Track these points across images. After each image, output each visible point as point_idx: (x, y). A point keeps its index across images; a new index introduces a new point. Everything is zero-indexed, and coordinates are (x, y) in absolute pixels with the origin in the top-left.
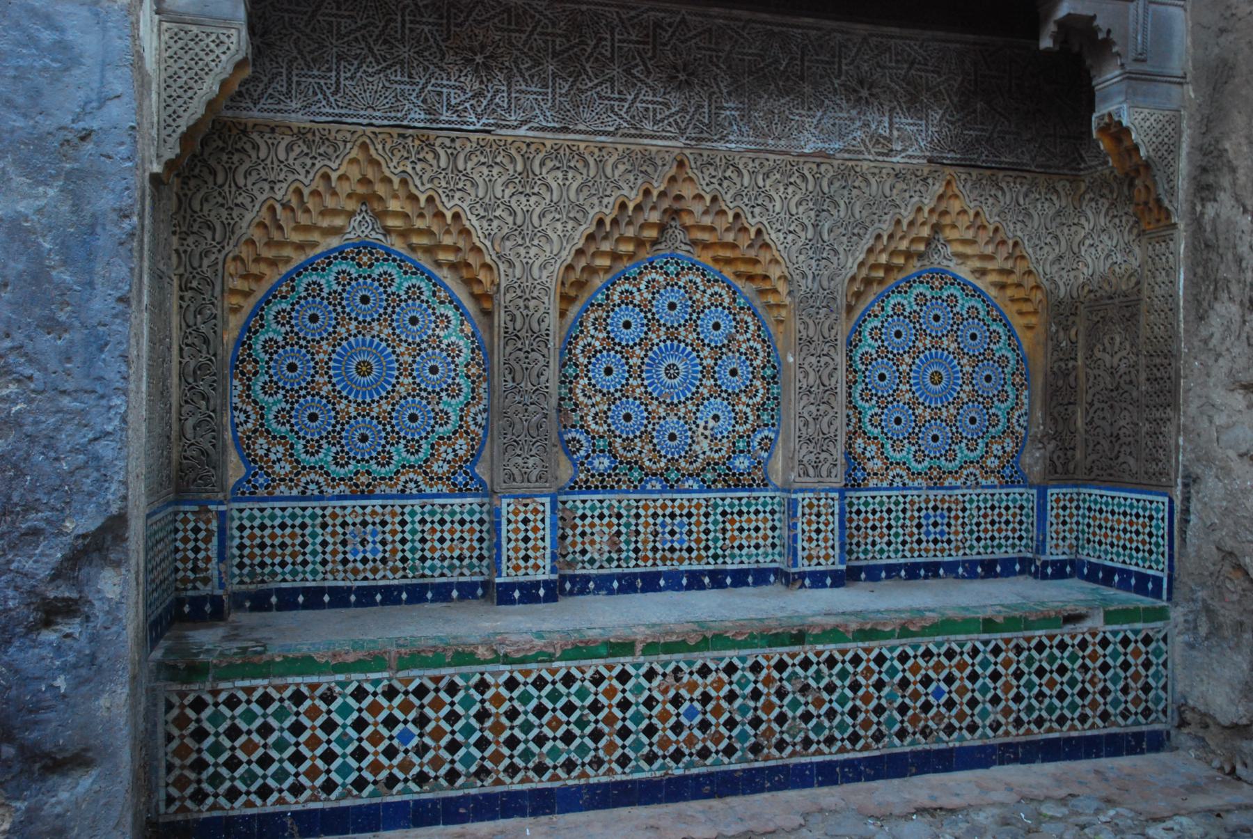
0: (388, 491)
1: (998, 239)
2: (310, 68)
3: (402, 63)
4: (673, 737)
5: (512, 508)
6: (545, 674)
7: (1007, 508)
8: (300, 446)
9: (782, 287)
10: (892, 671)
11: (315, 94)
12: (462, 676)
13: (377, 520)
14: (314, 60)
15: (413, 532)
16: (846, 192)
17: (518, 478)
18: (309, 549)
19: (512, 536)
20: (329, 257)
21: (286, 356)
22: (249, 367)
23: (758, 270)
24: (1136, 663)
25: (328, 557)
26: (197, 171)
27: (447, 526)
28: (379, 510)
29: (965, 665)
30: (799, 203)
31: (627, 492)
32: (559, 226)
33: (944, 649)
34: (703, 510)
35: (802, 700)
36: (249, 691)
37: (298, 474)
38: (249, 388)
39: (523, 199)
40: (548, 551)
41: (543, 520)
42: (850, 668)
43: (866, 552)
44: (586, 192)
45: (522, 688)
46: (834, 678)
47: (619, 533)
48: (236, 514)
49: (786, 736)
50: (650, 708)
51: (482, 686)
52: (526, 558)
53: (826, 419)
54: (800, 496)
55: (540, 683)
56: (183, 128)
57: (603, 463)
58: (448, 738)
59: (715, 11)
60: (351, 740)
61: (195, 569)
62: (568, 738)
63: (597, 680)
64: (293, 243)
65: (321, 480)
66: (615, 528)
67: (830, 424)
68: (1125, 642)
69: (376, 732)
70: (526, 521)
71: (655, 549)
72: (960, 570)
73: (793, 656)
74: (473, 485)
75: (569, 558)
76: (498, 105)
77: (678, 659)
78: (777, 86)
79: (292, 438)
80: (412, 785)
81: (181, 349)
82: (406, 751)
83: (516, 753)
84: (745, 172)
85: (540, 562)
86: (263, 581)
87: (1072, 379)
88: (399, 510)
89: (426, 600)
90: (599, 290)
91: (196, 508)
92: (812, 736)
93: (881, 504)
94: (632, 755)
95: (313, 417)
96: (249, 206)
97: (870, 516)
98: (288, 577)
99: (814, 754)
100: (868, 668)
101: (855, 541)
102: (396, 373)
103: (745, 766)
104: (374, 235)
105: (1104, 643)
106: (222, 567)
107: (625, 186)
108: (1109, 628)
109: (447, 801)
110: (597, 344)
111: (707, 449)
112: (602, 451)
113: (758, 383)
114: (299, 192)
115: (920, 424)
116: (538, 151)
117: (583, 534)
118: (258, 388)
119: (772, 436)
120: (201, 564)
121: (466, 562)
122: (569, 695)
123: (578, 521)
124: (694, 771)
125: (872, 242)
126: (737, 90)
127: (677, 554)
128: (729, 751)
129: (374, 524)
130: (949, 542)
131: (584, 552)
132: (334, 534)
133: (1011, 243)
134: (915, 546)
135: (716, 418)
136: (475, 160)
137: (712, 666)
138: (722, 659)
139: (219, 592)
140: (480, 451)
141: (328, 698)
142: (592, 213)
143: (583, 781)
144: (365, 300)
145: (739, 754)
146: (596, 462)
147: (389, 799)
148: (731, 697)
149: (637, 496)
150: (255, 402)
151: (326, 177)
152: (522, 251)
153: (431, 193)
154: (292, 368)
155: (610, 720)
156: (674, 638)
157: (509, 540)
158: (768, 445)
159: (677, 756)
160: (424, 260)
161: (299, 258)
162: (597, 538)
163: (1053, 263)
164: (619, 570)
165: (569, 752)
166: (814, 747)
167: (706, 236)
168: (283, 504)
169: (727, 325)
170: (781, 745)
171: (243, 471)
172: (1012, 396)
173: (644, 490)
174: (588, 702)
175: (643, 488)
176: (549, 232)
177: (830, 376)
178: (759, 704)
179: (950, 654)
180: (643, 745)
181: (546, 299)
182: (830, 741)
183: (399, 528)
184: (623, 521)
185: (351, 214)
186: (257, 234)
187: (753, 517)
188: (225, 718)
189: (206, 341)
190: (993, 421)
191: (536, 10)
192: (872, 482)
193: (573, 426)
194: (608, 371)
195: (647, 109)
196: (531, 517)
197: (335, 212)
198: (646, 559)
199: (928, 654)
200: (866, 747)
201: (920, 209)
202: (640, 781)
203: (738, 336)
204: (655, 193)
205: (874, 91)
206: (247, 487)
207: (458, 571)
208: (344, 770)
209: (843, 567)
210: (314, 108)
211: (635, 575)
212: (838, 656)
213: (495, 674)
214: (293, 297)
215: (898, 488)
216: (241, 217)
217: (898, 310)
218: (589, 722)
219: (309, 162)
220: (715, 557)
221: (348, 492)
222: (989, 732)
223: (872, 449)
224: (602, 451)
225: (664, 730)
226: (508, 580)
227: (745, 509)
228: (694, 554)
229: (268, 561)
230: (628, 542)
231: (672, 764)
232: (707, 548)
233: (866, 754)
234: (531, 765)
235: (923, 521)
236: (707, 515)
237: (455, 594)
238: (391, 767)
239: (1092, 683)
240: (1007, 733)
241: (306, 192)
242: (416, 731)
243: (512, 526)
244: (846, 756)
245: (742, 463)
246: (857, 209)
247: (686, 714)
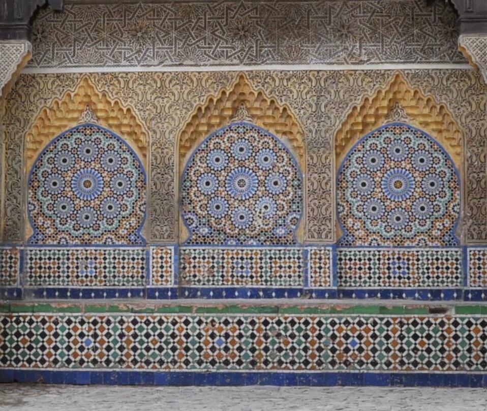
0: (98, 243)
2: (62, 46)
4: (211, 353)
6: (150, 318)
7: (447, 260)
9: (298, 137)
11: (64, 57)
12: (113, 317)
13: (93, 257)
14: (64, 42)
16: (334, 85)
18: (61, 270)
19: (155, 265)
21: (52, 179)
22: (36, 184)
23: (286, 129)
25: (70, 274)
27: (126, 261)
28: (94, 252)
29: (369, 330)
30: (308, 93)
32: (178, 112)
34: (259, 256)
35: (277, 341)
36: (25, 317)
37: (57, 234)
38: (35, 193)
39: (161, 100)
40: (173, 273)
41: (170, 258)
42: (303, 327)
43: (355, 282)
44: (192, 95)
45: (139, 324)
46: (295, 331)
47: (213, 267)
49: (269, 358)
50: (200, 338)
51: (122, 322)
52: (162, 276)
54: (309, 248)
55: (148, 323)
57: (205, 230)
58: (106, 344)
60: (65, 342)
61: (10, 276)
62: (161, 349)
64: (55, 126)
65: (67, 237)
66: (211, 265)
67: (327, 210)
69: (76, 339)
70: (162, 258)
71: (232, 276)
72: (417, 295)
73: (272, 318)
74: (139, 241)
75: (187, 279)
76: (148, 56)
77: (212, 316)
78: (294, 32)
79: (54, 217)
81: (6, 176)
82: (88, 349)
83: (137, 354)
85: (169, 279)
86: (40, 285)
88: (103, 252)
89: (115, 297)
90: (203, 143)
91: (10, 248)
92: (283, 359)
93: (364, 255)
94: (191, 360)
95: (64, 207)
96: (35, 110)
97: (358, 262)
98: (52, 283)
100: (313, 328)
101: (348, 275)
102: (102, 186)
103: (248, 371)
104: (92, 120)
106: (22, 275)
108: (458, 316)
110: (202, 170)
111: (261, 224)
112: (204, 224)
113: (290, 189)
114: (57, 103)
115: (388, 211)
116: (168, 76)
117: (194, 267)
120: (13, 274)
121: (135, 279)
122: (161, 329)
123: (192, 260)
124: (222, 371)
125: (350, 111)
126: (270, 37)
127: (244, 279)
128: (240, 363)
129: (91, 259)
130: (409, 278)
131: (195, 276)
132: (73, 263)
133: (438, 107)
134: (387, 280)
135: (266, 207)
136: (137, 83)
137: (230, 320)
139: (20, 287)
140: (143, 223)
141: (56, 323)
142: (195, 105)
143: (167, 370)
144: (88, 151)
145: (244, 364)
146: (201, 230)
147: (81, 370)
148: (240, 336)
149: (223, 248)
150: (38, 200)
151: (69, 95)
152: (160, 125)
153: (116, 100)
154: (55, 184)
155: (180, 342)
156: (211, 306)
157: (153, 267)
158: (295, 221)
159: (213, 363)
160: (116, 131)
161: (58, 133)
162: (202, 269)
163: (467, 117)
164: (214, 286)
165: (161, 356)
166: (284, 365)
167: (258, 113)
168: (50, 248)
169: (272, 158)
170: (266, 362)
172: (448, 194)
173: (226, 245)
174: (170, 333)
175: (226, 243)
176: (174, 116)
178: (255, 341)
179: (360, 324)
180: (196, 356)
181: (172, 148)
182: (293, 363)
183: (103, 261)
184: (215, 260)
185: (82, 111)
186: (38, 123)
188: (15, 328)
189: (16, 172)
190: (436, 209)
191: (166, 8)
192: (358, 243)
193: (190, 212)
194: (208, 184)
195: (223, 51)
197: (73, 111)
198: (228, 281)
199: (347, 323)
200: (313, 368)
201: (379, 92)
202: (194, 373)
203: (278, 164)
204: (228, 93)
205: (350, 30)
206: (34, 240)
207: (131, 283)
208: (62, 355)
209: (335, 288)
210: (64, 64)
211: (222, 289)
212: (296, 320)
213: (128, 317)
214: (55, 151)
215: (374, 247)
216: (32, 115)
217: (373, 148)
218: (170, 343)
219: (61, 89)
220: (266, 281)
221: (79, 243)
222: (385, 367)
224: (204, 224)
225: (206, 349)
226: (153, 287)
227: (282, 256)
228: (254, 279)
229: (43, 275)
230: (218, 272)
231: (211, 366)
232: (261, 276)
233: (313, 372)
234: (143, 360)
235: (391, 266)
236: (261, 259)
239: (448, 344)
240: (395, 368)
241: (60, 102)
243: (155, 260)
245: (280, 232)
246: (341, 94)
247: (217, 343)
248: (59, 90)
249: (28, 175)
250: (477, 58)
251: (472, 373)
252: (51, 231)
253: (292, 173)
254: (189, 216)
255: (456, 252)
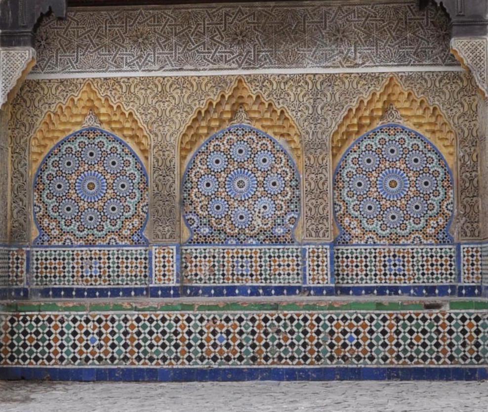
0: (102, 243)
1: (424, 106)
2: (65, 52)
3: (105, 46)
5: (157, 251)
6: (153, 316)
7: (441, 257)
8: (63, 222)
9: (296, 138)
10: (325, 326)
11: (68, 63)
12: (117, 315)
13: (97, 257)
15: (114, 263)
17: (160, 237)
18: (66, 270)
20: (75, 136)
22: (41, 187)
23: (285, 131)
24: (471, 331)
25: (75, 274)
26: (19, 102)
27: (129, 260)
28: (98, 252)
29: (366, 326)
30: (304, 96)
31: (218, 245)
32: (179, 115)
33: (354, 316)
34: (258, 255)
35: (277, 337)
36: (31, 316)
37: (61, 235)
38: (41, 196)
39: (162, 104)
40: (175, 272)
41: (172, 257)
42: (302, 323)
43: (352, 279)
45: (143, 322)
46: (294, 328)
47: (214, 266)
48: (35, 253)
49: (269, 354)
51: (126, 320)
52: (164, 275)
53: (321, 207)
54: (307, 247)
55: (151, 320)
56: (9, 91)
57: (206, 230)
59: (257, 4)
60: (71, 340)
61: (17, 276)
62: (164, 346)
63: (177, 321)
65: (72, 238)
66: (212, 263)
68: (463, 319)
69: (81, 337)
70: (164, 257)
71: (233, 275)
72: (412, 291)
74: (142, 241)
75: (189, 277)
76: (149, 61)
77: (214, 313)
78: (290, 37)
79: (59, 219)
80: (96, 362)
82: (93, 347)
84: (274, 82)
85: (171, 278)
87: (475, 182)
88: (107, 252)
90: (203, 145)
91: (17, 249)
92: (282, 355)
94: (193, 356)
97: (354, 260)
98: (57, 283)
99: (284, 364)
101: (345, 273)
102: (105, 188)
103: (248, 367)
104: (95, 124)
105: (450, 319)
106: (28, 275)
107: (211, 94)
109: (111, 370)
110: (202, 171)
111: (260, 223)
112: (205, 224)
113: (288, 189)
114: (61, 108)
117: (196, 266)
118: (45, 196)
119: (296, 216)
120: (19, 274)
121: (138, 278)
122: (164, 326)
123: (193, 259)
125: (346, 113)
126: (268, 41)
127: (245, 277)
128: (240, 359)
130: (404, 275)
131: (196, 275)
132: (77, 263)
133: (431, 108)
134: (383, 277)
135: (265, 207)
136: (139, 87)
137: (231, 318)
138: (236, 315)
139: (26, 287)
140: (145, 224)
141: (62, 321)
143: (170, 367)
144: (91, 154)
145: (245, 360)
146: (202, 230)
147: (86, 367)
149: (224, 247)
151: (73, 100)
152: (161, 128)
153: (118, 104)
156: (213, 304)
157: (156, 266)
158: (294, 221)
159: (215, 359)
160: (118, 135)
161: (62, 137)
162: (203, 268)
163: (459, 118)
164: (215, 285)
165: (164, 353)
166: (284, 361)
167: (256, 115)
168: (55, 249)
169: (270, 160)
170: (266, 358)
171: (38, 234)
172: (442, 193)
173: (227, 244)
174: (173, 330)
175: (227, 243)
176: (174, 119)
177: (323, 184)
178: (255, 337)
179: (357, 320)
180: (198, 352)
181: (173, 151)
182: (292, 358)
183: (107, 261)
184: (216, 259)
185: (85, 115)
186: (43, 127)
187: (286, 259)
189: (22, 176)
192: (355, 241)
193: (191, 212)
194: (208, 185)
196: (166, 255)
197: (76, 115)
198: (228, 279)
199: (344, 319)
201: (374, 94)
202: (197, 369)
203: (276, 165)
204: (227, 97)
206: (40, 241)
208: (68, 353)
209: (333, 285)
210: (67, 70)
211: (223, 287)
212: (295, 317)
213: (132, 315)
214: (60, 155)
215: (370, 245)
216: (37, 120)
217: (369, 148)
218: (173, 340)
220: (266, 279)
221: (84, 243)
222: (381, 361)
223: (354, 223)
224: (205, 224)
225: (208, 346)
226: (156, 285)
227: (281, 255)
228: (254, 277)
230: (219, 270)
231: (212, 362)
233: (312, 367)
234: (147, 357)
235: (387, 263)
236: (260, 257)
237: (133, 293)
238: (87, 353)
240: (392, 363)
241: (64, 107)
242: (97, 338)
243: (157, 260)
244: (301, 367)
245: (279, 231)
246: (337, 96)
248: (63, 95)
249: (33, 178)
250: (469, 60)
251: (467, 366)
252: (56, 232)
253: (289, 174)
254: (191, 216)
255: (450, 249)
